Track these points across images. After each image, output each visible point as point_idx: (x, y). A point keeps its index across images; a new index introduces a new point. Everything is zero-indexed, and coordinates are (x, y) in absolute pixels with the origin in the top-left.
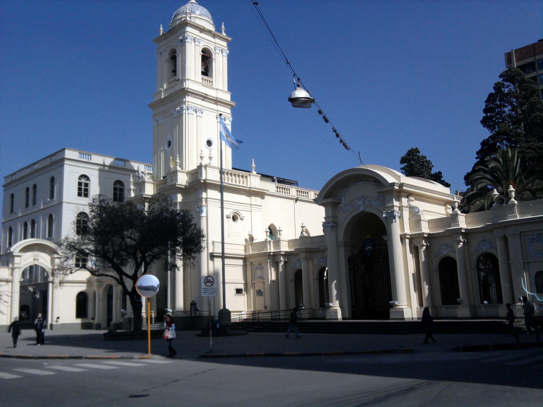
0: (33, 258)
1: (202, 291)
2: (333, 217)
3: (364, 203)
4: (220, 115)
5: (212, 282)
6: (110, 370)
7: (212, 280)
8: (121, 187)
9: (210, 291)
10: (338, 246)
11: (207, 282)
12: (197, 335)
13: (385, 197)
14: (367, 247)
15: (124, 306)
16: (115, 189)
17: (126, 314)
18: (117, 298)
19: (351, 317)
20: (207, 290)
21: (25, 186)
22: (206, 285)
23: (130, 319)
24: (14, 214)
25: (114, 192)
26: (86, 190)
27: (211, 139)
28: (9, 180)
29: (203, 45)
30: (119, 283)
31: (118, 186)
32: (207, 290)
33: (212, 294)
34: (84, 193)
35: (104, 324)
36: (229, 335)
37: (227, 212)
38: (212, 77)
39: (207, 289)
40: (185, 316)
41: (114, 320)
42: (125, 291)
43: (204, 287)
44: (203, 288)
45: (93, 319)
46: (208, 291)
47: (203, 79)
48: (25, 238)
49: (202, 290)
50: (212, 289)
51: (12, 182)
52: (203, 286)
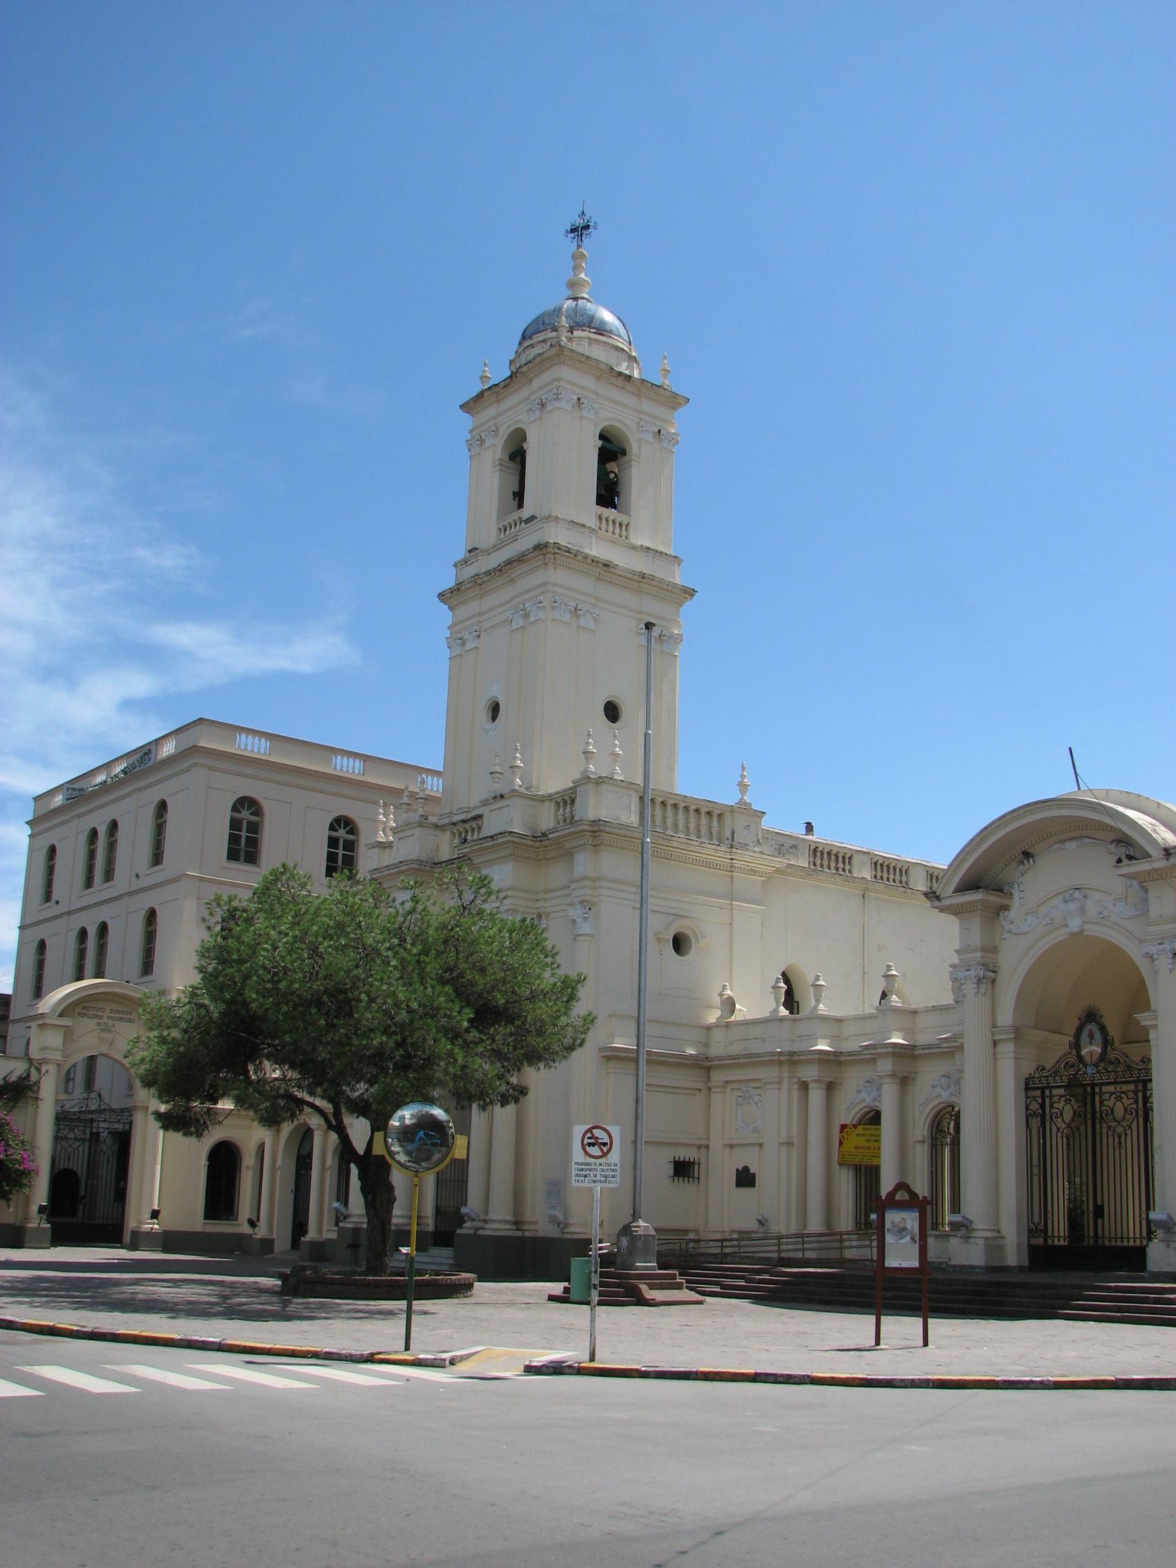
2: (983, 949)
3: (1082, 909)
4: (649, 626)
5: (605, 1144)
6: (291, 1390)
8: (351, 837)
9: (599, 1173)
10: (995, 1043)
11: (589, 1144)
12: (552, 1298)
13: (1146, 891)
14: (1085, 1048)
15: (343, 1195)
17: (345, 1218)
18: (323, 1168)
19: (1026, 1262)
20: (590, 1170)
21: (86, 824)
23: (356, 1231)
24: (52, 903)
25: (329, 864)
26: (254, 843)
27: (617, 698)
30: (330, 1127)
31: (341, 833)
32: (590, 1170)
33: (605, 1182)
34: (246, 852)
35: (282, 1243)
36: (642, 1302)
37: (655, 923)
38: (627, 512)
39: (589, 1164)
40: (519, 1234)
41: (311, 1235)
42: (346, 1151)
44: (579, 1161)
45: (252, 1224)
46: (592, 1173)
48: (80, 977)
49: (574, 1166)
50: (605, 1168)
51: (476, 581)
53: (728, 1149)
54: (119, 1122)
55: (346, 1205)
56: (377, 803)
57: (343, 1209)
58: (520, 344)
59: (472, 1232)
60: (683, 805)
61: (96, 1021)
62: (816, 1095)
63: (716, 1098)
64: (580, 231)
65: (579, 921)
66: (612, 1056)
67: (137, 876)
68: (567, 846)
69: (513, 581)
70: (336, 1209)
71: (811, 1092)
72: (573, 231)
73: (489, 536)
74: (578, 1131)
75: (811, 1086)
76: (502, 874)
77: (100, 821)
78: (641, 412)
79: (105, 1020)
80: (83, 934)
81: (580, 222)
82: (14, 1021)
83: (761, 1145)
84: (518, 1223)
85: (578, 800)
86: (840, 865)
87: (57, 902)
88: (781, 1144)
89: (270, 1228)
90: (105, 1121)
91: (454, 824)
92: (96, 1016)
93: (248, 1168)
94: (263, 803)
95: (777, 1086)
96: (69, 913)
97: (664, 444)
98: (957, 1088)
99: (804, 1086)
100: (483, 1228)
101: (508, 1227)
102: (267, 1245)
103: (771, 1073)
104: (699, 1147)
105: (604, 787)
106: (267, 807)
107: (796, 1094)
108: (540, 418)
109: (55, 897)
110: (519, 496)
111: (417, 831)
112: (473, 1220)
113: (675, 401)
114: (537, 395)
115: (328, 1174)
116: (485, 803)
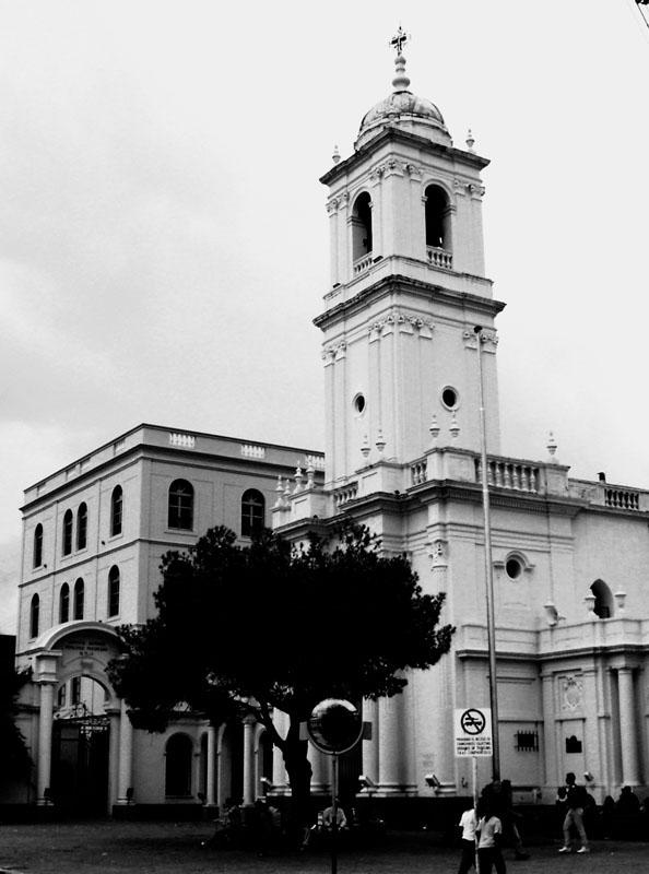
0: (78, 661)
1: (456, 746)
5: (480, 723)
7: (481, 719)
11: (468, 724)
15: (267, 770)
16: (245, 509)
22: (465, 731)
24: (42, 566)
28: (33, 496)
29: (429, 177)
40: (404, 795)
43: (461, 737)
47: (430, 254)
49: (456, 742)
52: (459, 732)
53: (559, 724)
54: (99, 725)
55: (270, 778)
56: (277, 478)
57: (269, 783)
58: (361, 129)
59: (367, 795)
60: (515, 465)
61: (79, 651)
62: (624, 680)
63: (548, 685)
64: (398, 42)
65: (435, 556)
66: (467, 658)
67: (103, 543)
68: (423, 500)
69: (368, 306)
70: (264, 783)
71: (620, 677)
72: (394, 42)
73: (347, 275)
74: (458, 714)
75: (620, 672)
76: (375, 525)
77: (72, 504)
78: (455, 173)
79: (86, 650)
80: (65, 588)
81: (397, 35)
82: (18, 655)
83: (584, 720)
84: (403, 787)
85: (428, 466)
86: (629, 502)
87: (45, 566)
88: (600, 718)
89: (216, 800)
90: (90, 725)
91: (336, 490)
92: (79, 648)
93: (197, 755)
94: (193, 483)
95: (593, 674)
96: (54, 573)
97: (475, 196)
98: (261, 727)
99: (614, 673)
100: (376, 792)
101: (395, 790)
102: (214, 811)
103: (588, 665)
104: (536, 723)
105: (447, 455)
106: (197, 487)
107: (609, 679)
108: (380, 183)
109: (43, 562)
110: (367, 244)
111: (309, 497)
112: (368, 786)
113: (480, 164)
114: (377, 166)
115: (257, 756)
116: (359, 472)
